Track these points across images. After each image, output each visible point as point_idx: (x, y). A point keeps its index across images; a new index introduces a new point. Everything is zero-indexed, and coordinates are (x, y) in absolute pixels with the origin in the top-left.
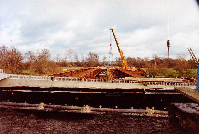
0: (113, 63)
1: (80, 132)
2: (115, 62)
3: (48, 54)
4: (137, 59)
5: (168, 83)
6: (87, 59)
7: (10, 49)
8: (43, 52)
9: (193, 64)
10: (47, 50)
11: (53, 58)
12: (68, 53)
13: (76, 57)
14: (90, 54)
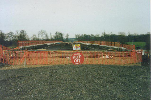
0: (74, 39)
1: (6, 86)
2: (74, 38)
3: (25, 34)
4: (91, 36)
5: (100, 51)
6: (55, 37)
7: (83, 35)
8: (21, 33)
9: (144, 38)
10: (24, 31)
11: (30, 36)
12: (40, 33)
13: (46, 35)
14: (57, 33)
